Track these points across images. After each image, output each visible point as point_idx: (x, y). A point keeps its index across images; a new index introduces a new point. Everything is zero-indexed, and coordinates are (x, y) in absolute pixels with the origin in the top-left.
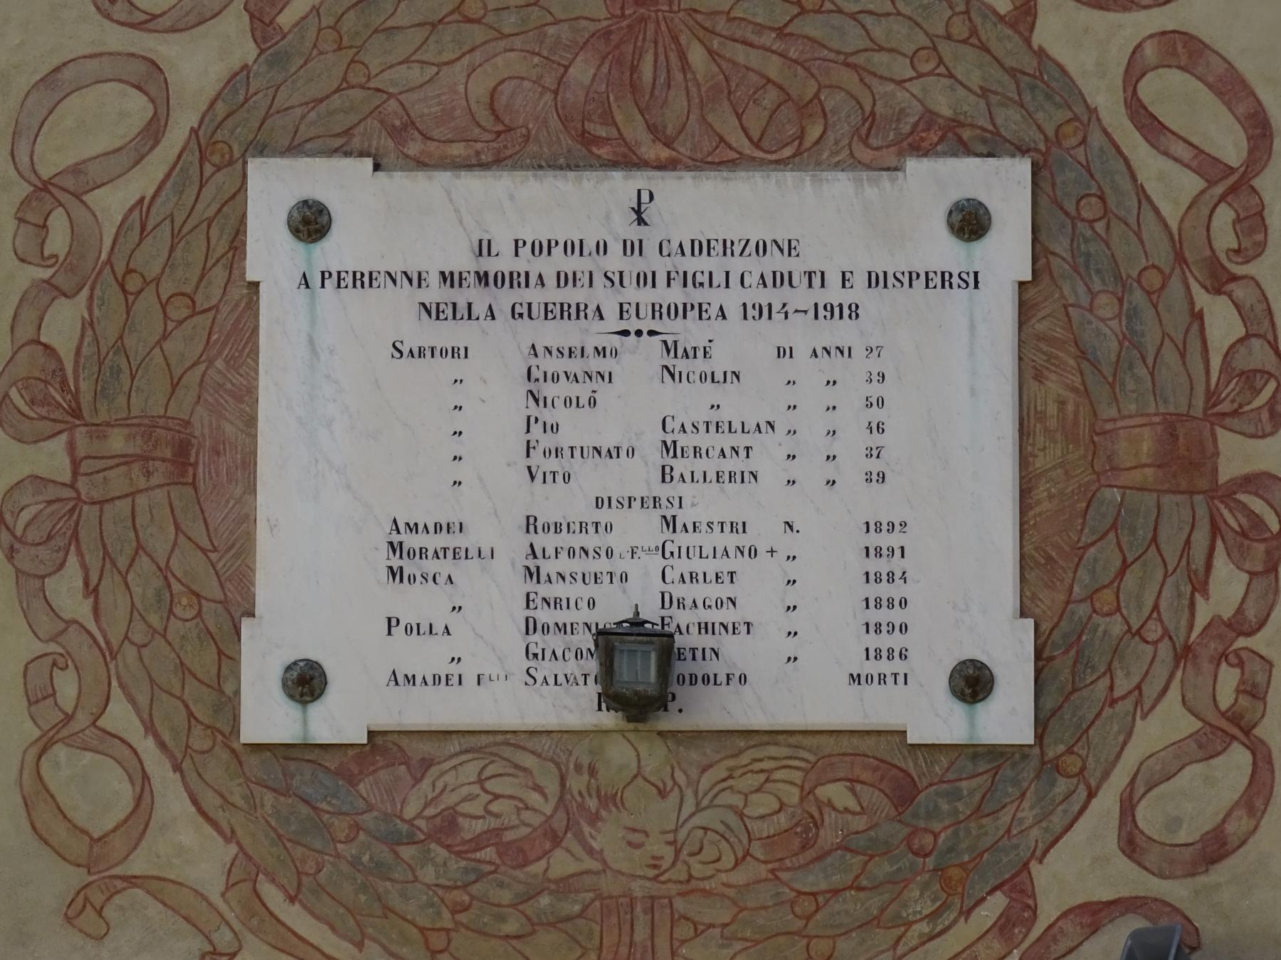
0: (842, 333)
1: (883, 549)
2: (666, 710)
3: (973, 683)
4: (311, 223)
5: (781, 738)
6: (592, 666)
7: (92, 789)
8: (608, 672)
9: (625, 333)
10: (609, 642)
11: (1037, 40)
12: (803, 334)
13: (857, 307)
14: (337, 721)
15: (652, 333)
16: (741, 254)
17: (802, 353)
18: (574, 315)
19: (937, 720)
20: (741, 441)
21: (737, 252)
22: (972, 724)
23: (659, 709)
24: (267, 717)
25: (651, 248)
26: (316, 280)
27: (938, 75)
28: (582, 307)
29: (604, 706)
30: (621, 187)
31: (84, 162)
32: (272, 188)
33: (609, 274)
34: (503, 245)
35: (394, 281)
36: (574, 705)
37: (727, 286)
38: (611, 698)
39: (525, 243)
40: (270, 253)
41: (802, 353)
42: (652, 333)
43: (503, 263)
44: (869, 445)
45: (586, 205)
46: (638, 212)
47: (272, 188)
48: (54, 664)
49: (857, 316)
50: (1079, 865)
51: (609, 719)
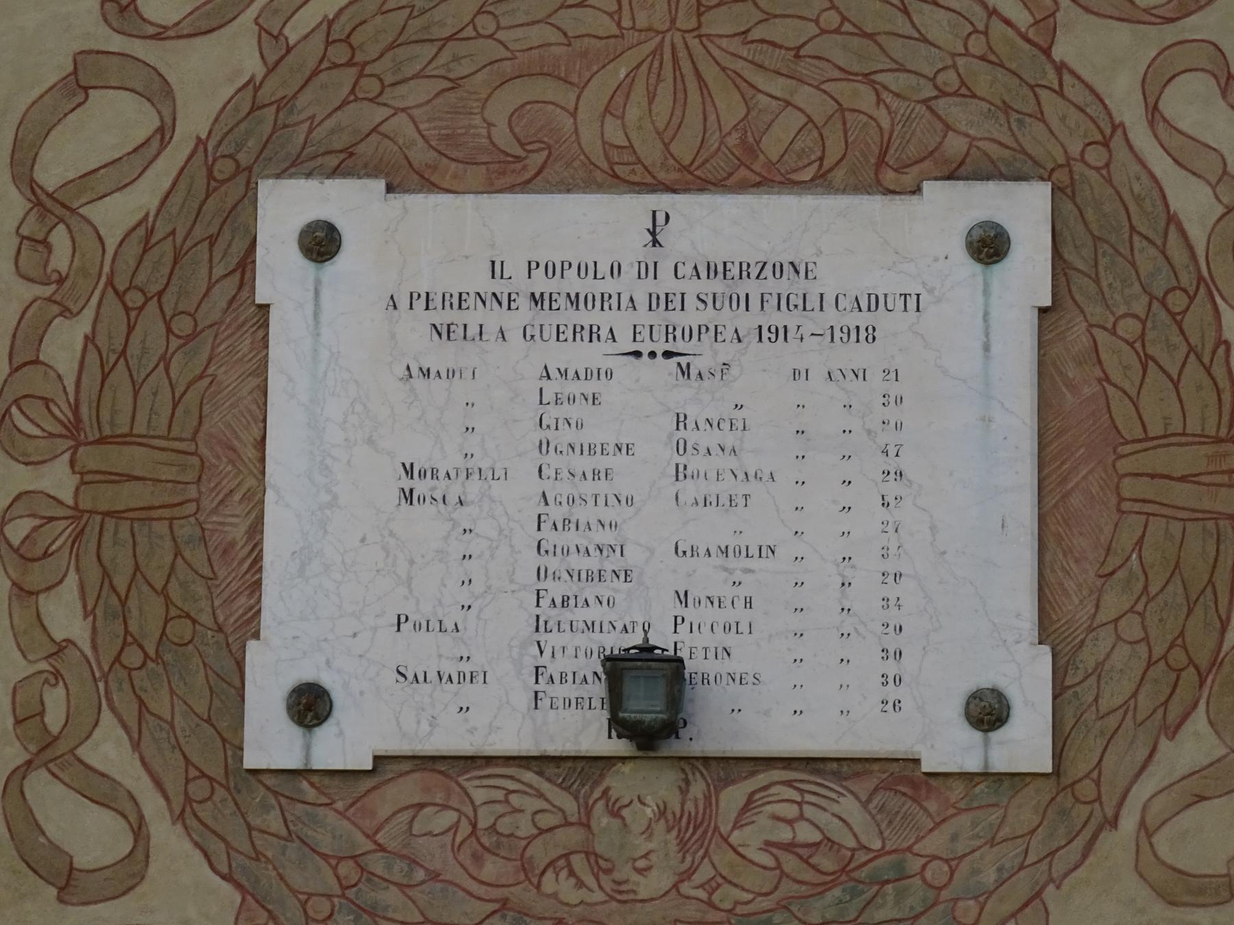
0: (859, 356)
2: (677, 737)
3: (988, 712)
4: (321, 243)
5: (876, 767)
6: (598, 690)
8: (615, 699)
9: (637, 354)
10: (620, 669)
11: (1058, 53)
12: (816, 356)
13: (874, 329)
14: (342, 745)
15: (668, 354)
16: (758, 277)
17: (818, 374)
18: (587, 338)
20: (601, 462)
21: (753, 275)
22: (307, 748)
23: (668, 737)
24: (270, 741)
25: (666, 270)
26: (403, 303)
27: (969, 89)
28: (595, 329)
29: (614, 733)
30: (633, 209)
33: (702, 297)
34: (515, 268)
35: (484, 303)
36: (590, 733)
37: (821, 309)
38: (619, 725)
39: (570, 265)
41: (818, 374)
42: (668, 354)
43: (520, 282)
44: (886, 468)
45: (592, 226)
46: (653, 233)
48: (46, 681)
49: (874, 338)
51: (620, 747)
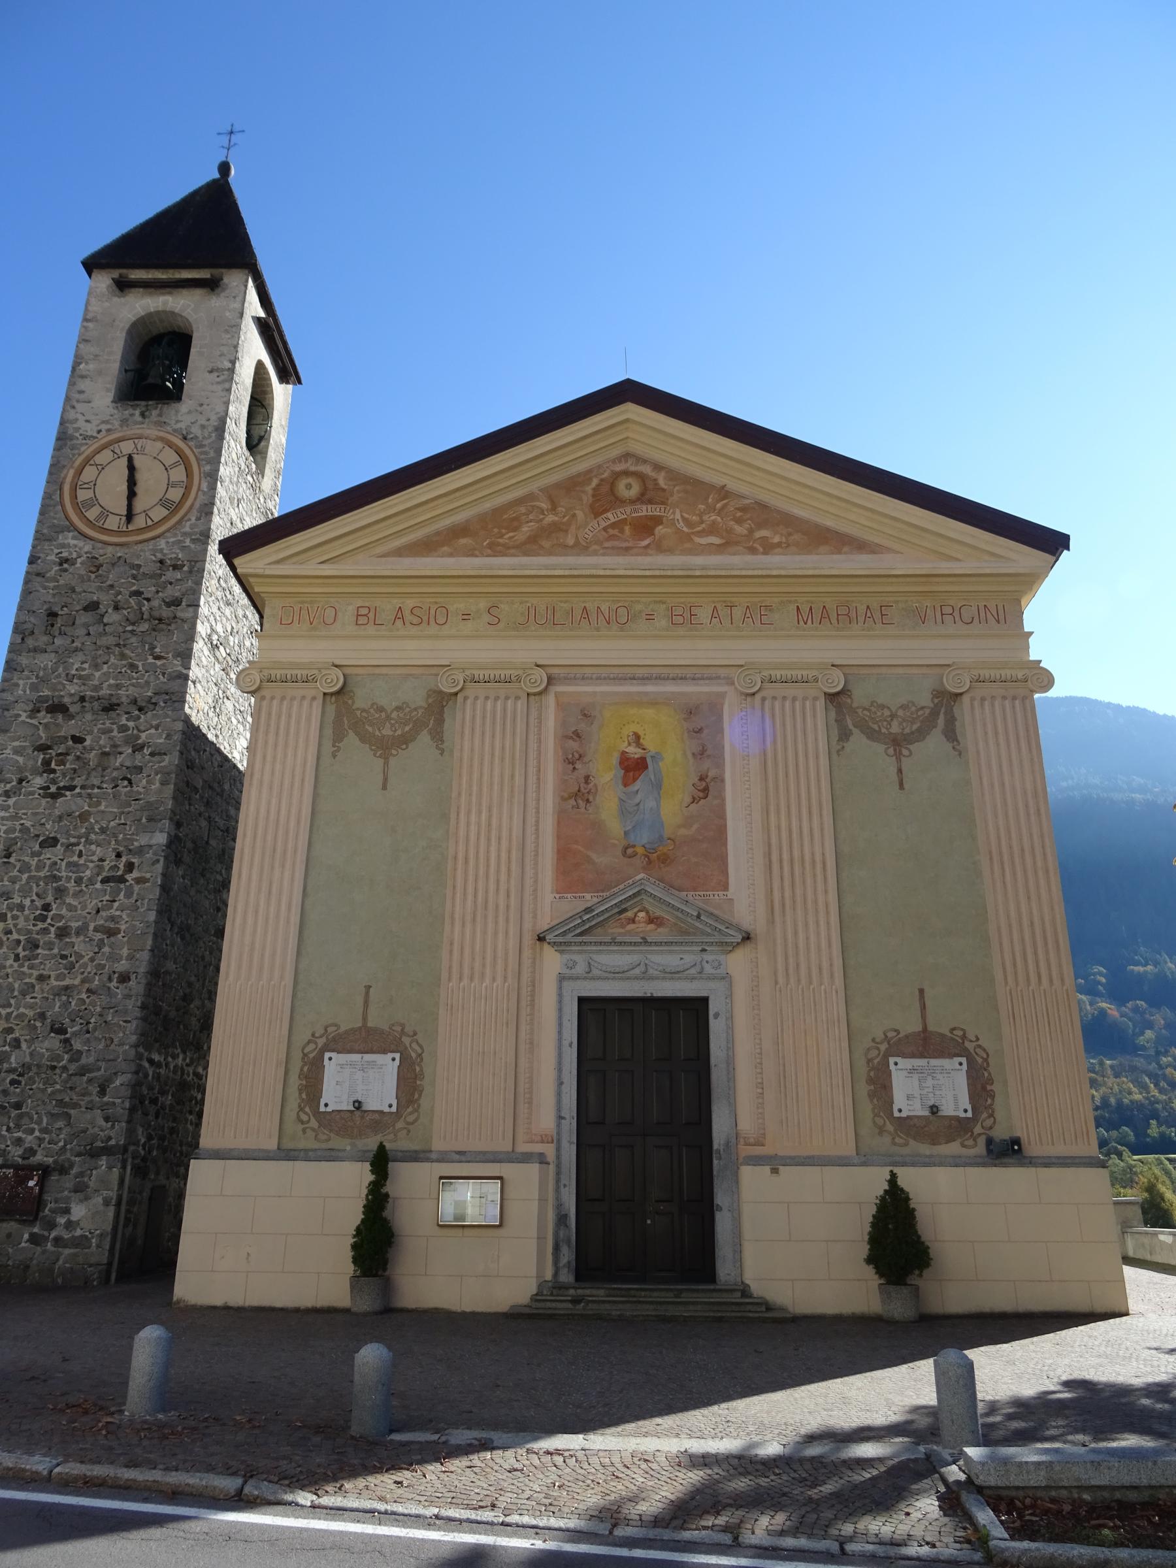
1: (956, 1098)
7: (880, 1121)
19: (963, 1115)
24: (896, 1114)
31: (285, 1154)
32: (327, 1055)
40: (892, 1067)
47: (892, 1060)
50: (978, 1129)
